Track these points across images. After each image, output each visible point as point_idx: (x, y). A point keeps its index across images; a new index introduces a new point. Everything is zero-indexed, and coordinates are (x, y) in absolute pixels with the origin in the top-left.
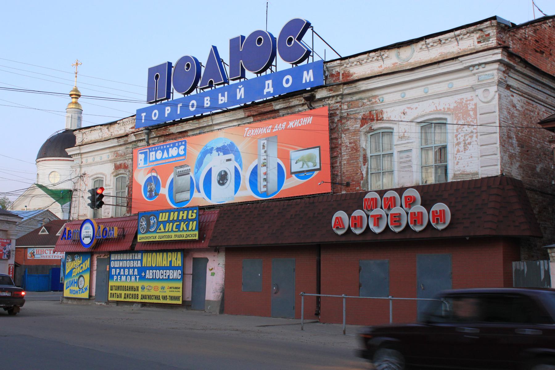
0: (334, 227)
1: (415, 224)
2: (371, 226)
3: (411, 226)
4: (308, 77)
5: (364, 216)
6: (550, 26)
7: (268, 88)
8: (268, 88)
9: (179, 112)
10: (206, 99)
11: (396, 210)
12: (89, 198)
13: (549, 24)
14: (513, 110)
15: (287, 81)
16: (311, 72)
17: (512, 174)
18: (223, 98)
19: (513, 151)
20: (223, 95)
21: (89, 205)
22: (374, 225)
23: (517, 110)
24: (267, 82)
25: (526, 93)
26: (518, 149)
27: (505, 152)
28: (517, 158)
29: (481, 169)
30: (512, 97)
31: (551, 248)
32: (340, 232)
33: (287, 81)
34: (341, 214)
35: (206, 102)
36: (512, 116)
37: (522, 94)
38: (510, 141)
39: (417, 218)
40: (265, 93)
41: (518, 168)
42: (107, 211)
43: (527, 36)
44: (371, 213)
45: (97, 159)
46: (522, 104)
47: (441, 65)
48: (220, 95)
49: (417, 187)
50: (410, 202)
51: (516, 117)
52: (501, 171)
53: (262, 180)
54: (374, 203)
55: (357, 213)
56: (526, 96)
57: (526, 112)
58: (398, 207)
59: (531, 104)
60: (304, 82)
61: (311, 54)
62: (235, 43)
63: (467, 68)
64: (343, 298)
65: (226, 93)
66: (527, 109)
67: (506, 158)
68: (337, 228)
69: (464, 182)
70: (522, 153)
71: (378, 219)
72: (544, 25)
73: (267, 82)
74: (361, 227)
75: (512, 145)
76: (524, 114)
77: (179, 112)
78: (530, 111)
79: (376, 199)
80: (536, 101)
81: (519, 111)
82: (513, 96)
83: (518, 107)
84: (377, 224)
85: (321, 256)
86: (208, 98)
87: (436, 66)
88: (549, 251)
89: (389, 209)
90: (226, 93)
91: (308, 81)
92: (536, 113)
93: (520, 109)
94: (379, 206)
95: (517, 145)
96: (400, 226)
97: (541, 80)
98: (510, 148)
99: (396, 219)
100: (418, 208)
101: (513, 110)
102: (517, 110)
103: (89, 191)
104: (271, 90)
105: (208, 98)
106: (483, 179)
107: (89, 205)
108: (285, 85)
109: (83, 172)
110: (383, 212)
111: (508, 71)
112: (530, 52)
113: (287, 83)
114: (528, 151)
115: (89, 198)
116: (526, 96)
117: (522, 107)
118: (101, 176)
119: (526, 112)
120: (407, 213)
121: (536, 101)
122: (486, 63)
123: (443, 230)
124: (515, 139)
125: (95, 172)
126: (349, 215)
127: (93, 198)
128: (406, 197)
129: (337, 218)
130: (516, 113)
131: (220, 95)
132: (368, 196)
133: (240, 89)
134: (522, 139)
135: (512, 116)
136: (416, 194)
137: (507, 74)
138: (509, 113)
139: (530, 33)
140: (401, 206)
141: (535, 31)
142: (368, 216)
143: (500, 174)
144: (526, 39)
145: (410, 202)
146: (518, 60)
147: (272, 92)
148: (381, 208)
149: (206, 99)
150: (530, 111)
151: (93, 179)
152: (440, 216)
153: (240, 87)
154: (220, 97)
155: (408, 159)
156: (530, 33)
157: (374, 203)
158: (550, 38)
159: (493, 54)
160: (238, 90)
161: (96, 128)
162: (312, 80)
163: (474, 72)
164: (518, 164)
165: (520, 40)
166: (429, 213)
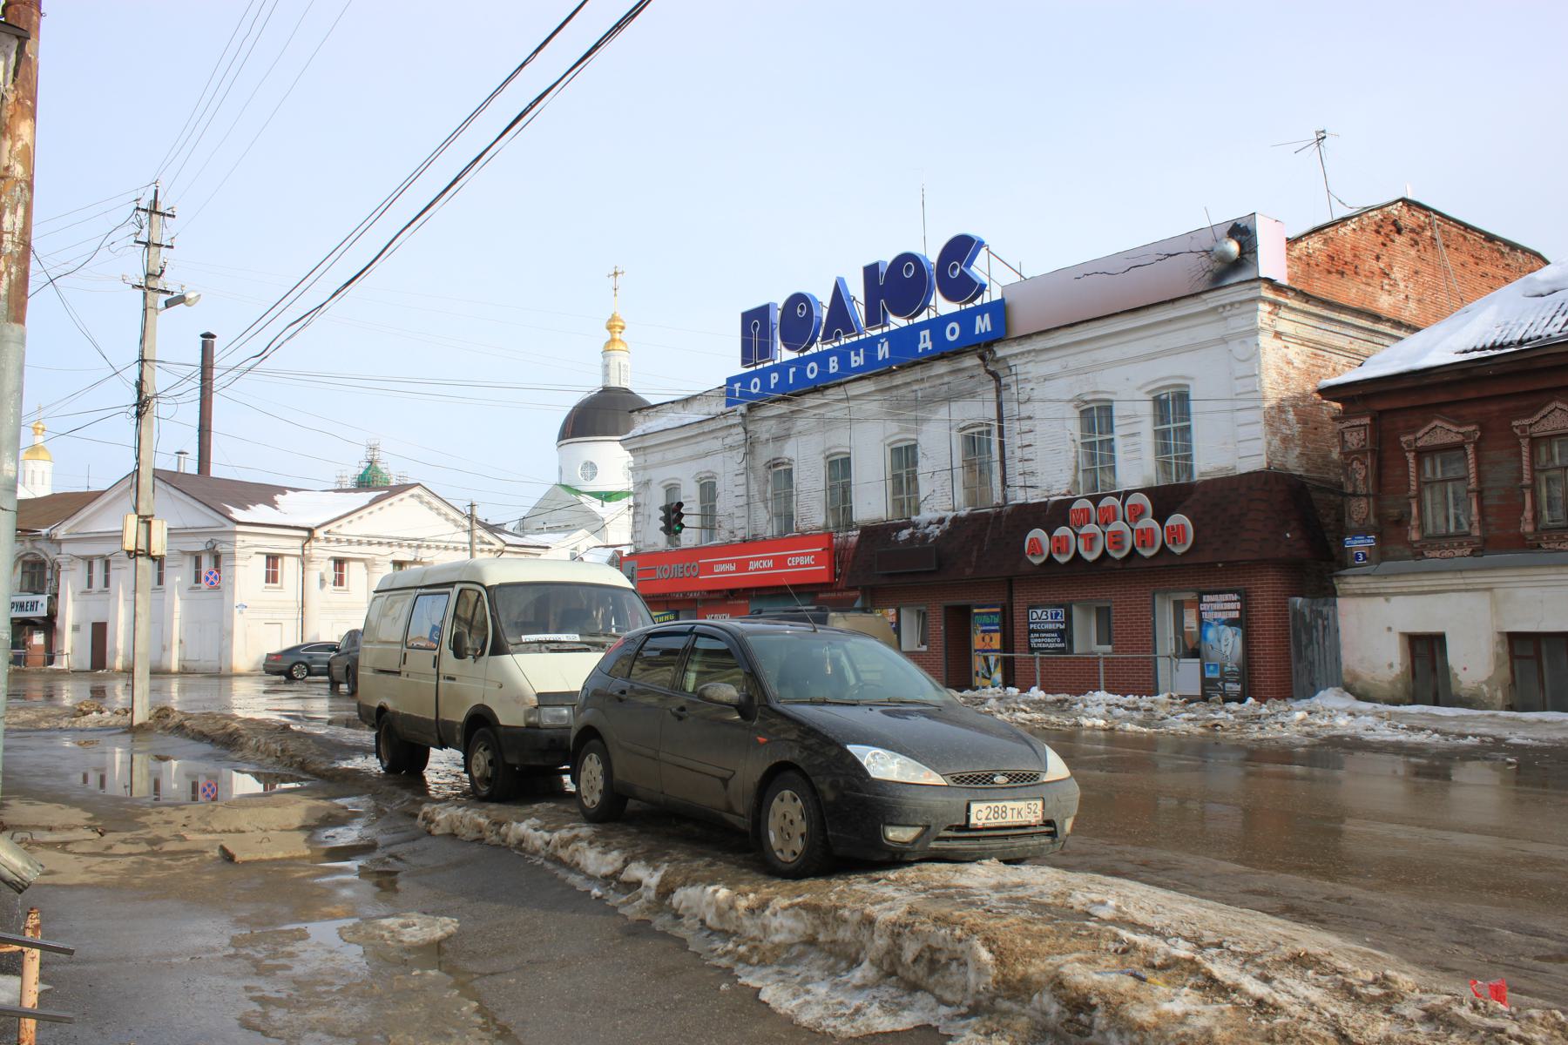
0: (1169, 543)
1: (1175, 543)
2: (1081, 551)
3: (1055, 556)
4: (983, 324)
5: (1072, 534)
6: (1354, 230)
7: (925, 342)
8: (925, 342)
9: (791, 382)
10: (831, 359)
11: (1113, 527)
12: (661, 519)
13: (1353, 226)
14: (1287, 369)
15: (953, 332)
16: (987, 316)
17: (1288, 466)
18: (857, 358)
19: (1288, 432)
20: (857, 354)
21: (662, 529)
22: (1085, 550)
23: (1294, 368)
24: (922, 333)
25: (1309, 340)
26: (1297, 428)
27: (1274, 434)
28: (1297, 442)
29: (1238, 461)
30: (1285, 350)
31: (1336, 576)
32: (1037, 561)
33: (953, 332)
34: (1038, 534)
35: (831, 365)
36: (1287, 378)
37: (1304, 342)
38: (1284, 417)
39: (1145, 537)
40: (920, 351)
41: (1297, 457)
42: (689, 535)
43: (1311, 251)
44: (1083, 531)
45: (670, 455)
46: (1305, 358)
47: (1178, 304)
48: (852, 353)
49: (1146, 491)
50: (1137, 513)
51: (1292, 379)
52: (1268, 463)
53: (1167, 371)
54: (1086, 516)
55: (1063, 531)
56: (1311, 345)
57: (1311, 368)
58: (1120, 522)
59: (1320, 356)
60: (977, 332)
61: (987, 288)
62: (871, 272)
63: (1215, 309)
64: (1035, 658)
65: (862, 350)
66: (1313, 365)
67: (1276, 442)
68: (1033, 554)
69: (1215, 481)
70: (1304, 434)
71: (1091, 539)
72: (1343, 229)
73: (922, 333)
74: (1068, 553)
75: (1286, 422)
76: (1308, 373)
77: (791, 382)
78: (1319, 367)
79: (1088, 509)
80: (1329, 349)
81: (1299, 369)
82: (1287, 347)
83: (1297, 363)
84: (1090, 549)
85: (1015, 594)
86: (835, 358)
87: (1169, 306)
88: (1335, 581)
89: (1107, 524)
90: (862, 350)
91: (983, 331)
92: (1330, 369)
93: (1300, 366)
94: (1093, 519)
95: (1295, 422)
96: (1122, 548)
97: (1336, 318)
98: (1283, 427)
99: (1117, 541)
100: (1148, 522)
101: (1287, 369)
102: (1294, 368)
103: (661, 508)
104: (929, 345)
105: (835, 358)
106: (1242, 475)
107: (662, 529)
108: (950, 338)
109: (647, 478)
110: (1096, 530)
111: (1276, 311)
112: (1317, 275)
113: (953, 333)
114: (1316, 429)
115: (661, 519)
116: (1311, 345)
117: (1304, 362)
118: (678, 482)
119: (1311, 368)
120: (1104, 533)
121: (1329, 349)
122: (1241, 302)
123: (1183, 554)
124: (1292, 413)
125: (673, 476)
126: (1050, 534)
127: (666, 519)
128: (1130, 506)
129: (1032, 540)
130: (1293, 373)
131: (852, 353)
132: (1075, 506)
133: (883, 344)
134: (1304, 412)
135: (1287, 378)
136: (1145, 501)
137: (1277, 315)
138: (1280, 374)
139: (1317, 246)
140: (1124, 520)
141: (1326, 242)
142: (1076, 535)
143: (1265, 465)
144: (1309, 255)
145: (1137, 513)
146: (1291, 294)
147: (930, 348)
148: (1096, 523)
149: (831, 359)
150: (1319, 367)
151: (665, 487)
152: (1178, 532)
153: (882, 341)
154: (853, 358)
155: (1134, 447)
156: (1316, 245)
157: (1086, 516)
158: (1354, 248)
159: (1250, 289)
160: (879, 346)
161: (664, 407)
162: (989, 329)
163: (1225, 314)
164: (1298, 451)
165: (1299, 258)
166: (1162, 529)
